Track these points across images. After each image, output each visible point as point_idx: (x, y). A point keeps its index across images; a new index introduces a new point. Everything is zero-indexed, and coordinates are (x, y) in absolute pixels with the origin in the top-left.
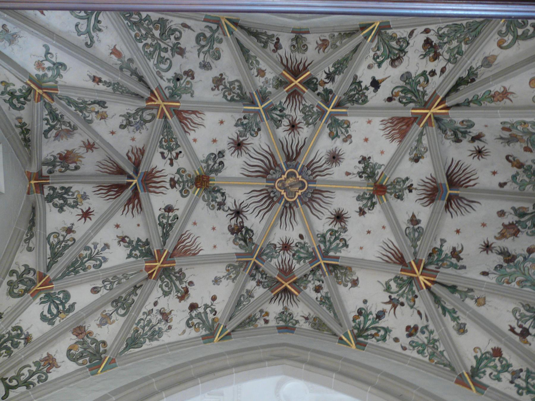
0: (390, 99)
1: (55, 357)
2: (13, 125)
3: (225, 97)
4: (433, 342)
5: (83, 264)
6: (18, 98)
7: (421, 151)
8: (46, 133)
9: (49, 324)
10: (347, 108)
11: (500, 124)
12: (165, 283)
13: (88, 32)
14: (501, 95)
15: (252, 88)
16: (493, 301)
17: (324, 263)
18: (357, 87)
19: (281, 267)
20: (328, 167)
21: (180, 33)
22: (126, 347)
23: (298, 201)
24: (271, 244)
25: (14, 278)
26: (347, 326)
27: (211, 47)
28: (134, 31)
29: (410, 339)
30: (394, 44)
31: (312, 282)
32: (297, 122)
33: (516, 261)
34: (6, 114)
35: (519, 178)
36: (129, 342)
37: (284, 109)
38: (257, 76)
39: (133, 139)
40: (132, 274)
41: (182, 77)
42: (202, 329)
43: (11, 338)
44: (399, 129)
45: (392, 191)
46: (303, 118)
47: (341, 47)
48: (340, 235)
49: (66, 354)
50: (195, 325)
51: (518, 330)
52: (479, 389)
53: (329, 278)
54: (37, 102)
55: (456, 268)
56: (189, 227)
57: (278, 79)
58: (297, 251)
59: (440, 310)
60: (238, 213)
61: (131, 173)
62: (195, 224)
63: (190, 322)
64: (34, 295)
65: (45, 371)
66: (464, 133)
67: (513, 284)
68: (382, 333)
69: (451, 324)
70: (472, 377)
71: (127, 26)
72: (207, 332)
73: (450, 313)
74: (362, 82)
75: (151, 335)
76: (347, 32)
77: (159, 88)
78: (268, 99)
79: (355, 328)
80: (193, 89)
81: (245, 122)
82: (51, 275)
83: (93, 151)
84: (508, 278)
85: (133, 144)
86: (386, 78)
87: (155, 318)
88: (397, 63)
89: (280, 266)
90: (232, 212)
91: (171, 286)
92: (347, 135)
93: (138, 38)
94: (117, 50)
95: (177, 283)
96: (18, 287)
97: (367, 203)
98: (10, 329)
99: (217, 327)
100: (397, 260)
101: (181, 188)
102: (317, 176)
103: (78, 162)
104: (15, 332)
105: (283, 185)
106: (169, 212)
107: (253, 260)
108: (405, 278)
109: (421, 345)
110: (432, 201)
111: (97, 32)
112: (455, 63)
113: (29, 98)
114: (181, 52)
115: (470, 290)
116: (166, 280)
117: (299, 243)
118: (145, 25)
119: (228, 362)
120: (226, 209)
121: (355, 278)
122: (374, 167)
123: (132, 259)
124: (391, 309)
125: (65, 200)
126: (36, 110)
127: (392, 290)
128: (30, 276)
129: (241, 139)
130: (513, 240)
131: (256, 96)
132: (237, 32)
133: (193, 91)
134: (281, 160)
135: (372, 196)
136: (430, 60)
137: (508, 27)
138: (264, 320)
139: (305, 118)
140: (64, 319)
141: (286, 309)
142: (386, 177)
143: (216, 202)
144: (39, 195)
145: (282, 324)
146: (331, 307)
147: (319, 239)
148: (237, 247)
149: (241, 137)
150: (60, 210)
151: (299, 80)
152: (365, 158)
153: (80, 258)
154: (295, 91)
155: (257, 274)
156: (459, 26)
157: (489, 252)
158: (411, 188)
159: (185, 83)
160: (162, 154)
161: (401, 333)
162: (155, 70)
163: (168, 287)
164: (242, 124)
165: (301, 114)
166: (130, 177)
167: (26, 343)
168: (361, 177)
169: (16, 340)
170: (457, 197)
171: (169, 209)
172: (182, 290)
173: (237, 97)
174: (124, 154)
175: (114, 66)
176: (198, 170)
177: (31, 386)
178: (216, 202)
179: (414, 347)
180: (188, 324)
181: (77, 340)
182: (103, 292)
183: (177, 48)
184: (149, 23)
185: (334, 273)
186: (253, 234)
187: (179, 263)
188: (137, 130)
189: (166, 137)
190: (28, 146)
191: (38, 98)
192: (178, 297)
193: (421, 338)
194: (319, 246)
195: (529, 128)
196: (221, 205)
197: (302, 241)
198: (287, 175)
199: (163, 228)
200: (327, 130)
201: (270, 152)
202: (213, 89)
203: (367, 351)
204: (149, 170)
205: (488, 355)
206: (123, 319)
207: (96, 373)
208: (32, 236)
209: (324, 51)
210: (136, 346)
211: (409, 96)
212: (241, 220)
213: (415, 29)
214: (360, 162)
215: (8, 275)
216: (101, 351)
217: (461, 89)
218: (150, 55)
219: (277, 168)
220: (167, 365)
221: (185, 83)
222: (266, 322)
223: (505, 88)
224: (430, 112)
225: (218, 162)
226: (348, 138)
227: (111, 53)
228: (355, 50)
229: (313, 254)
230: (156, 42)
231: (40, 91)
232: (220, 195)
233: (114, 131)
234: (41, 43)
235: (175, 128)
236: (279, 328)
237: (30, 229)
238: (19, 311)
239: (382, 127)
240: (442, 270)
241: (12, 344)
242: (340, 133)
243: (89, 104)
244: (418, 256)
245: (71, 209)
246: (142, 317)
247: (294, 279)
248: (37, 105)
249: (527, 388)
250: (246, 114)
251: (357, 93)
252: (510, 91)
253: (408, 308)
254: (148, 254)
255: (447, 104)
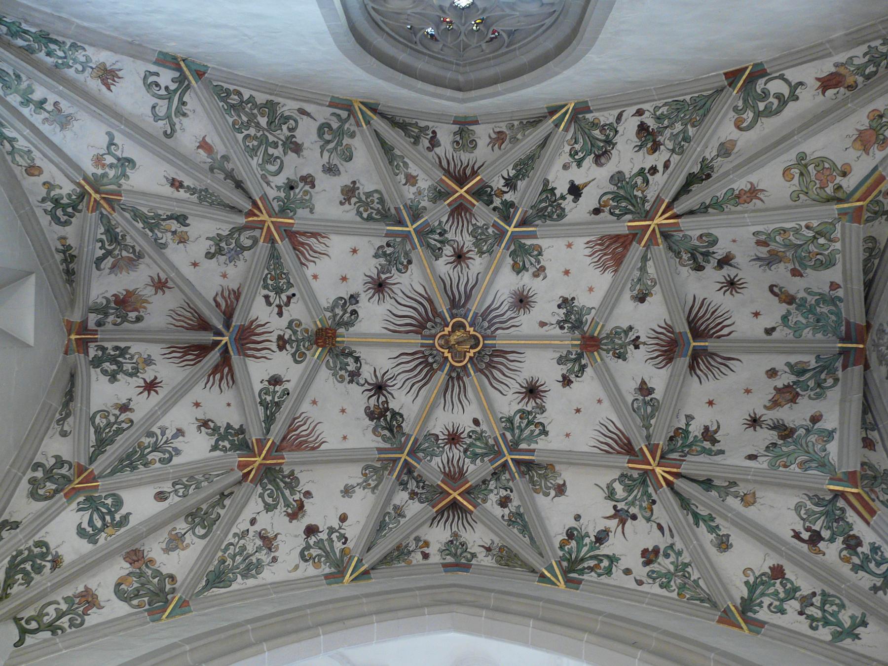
0: (597, 211)
1: (96, 593)
2: (53, 249)
3: (359, 214)
4: (682, 569)
5: (143, 456)
6: (64, 208)
7: (645, 284)
8: (99, 261)
9: (89, 542)
10: (537, 226)
11: (752, 236)
12: (269, 491)
13: (168, 117)
14: (748, 195)
15: (398, 201)
16: (766, 496)
17: (512, 459)
18: (549, 196)
19: (447, 469)
20: (513, 315)
21: (296, 121)
22: (207, 585)
23: (469, 366)
24: (430, 434)
25: (39, 474)
26: (550, 554)
27: (340, 143)
28: (232, 116)
29: (648, 568)
30: (597, 133)
31: (495, 492)
32: (465, 250)
33: (795, 436)
34: (45, 231)
35: (792, 319)
36: (212, 577)
37: (445, 231)
38: (405, 184)
39: (224, 276)
40: (218, 475)
41: (298, 184)
42: (325, 565)
43: (31, 557)
44: (613, 253)
45: (610, 347)
46: (474, 244)
47: (522, 140)
48: (535, 417)
49: (113, 590)
50: (314, 559)
51: (806, 535)
52: (752, 627)
53: (520, 482)
54: (92, 212)
55: (710, 455)
56: (305, 407)
57: (435, 189)
58: (470, 445)
59: (690, 518)
60: (379, 388)
61: (220, 327)
62: (314, 402)
63: (306, 553)
64: (71, 495)
65: (81, 612)
66: (707, 255)
67: (792, 467)
68: (605, 563)
69: (707, 537)
70: (743, 613)
71: (222, 109)
72: (333, 570)
73: (704, 521)
74: (556, 188)
75: (244, 570)
76: (532, 120)
77: (265, 197)
78: (423, 217)
79: (563, 558)
80: (313, 201)
81: (389, 250)
82: (96, 467)
83: (164, 293)
84: (785, 459)
85: (225, 283)
86: (590, 182)
87: (253, 544)
88: (603, 160)
89: (444, 468)
90: (370, 387)
91: (278, 496)
92: (538, 267)
93: (237, 127)
94: (207, 143)
95: (287, 492)
96: (45, 486)
97: (573, 367)
98: (31, 543)
99: (348, 562)
100: (622, 448)
101: (294, 350)
102: (497, 329)
103: (141, 310)
104: (38, 549)
105: (447, 342)
106: (275, 385)
107: (404, 456)
108: (635, 475)
109: (665, 575)
110: (670, 360)
111: (181, 118)
112: (681, 153)
113: (80, 207)
114: (297, 149)
115: (733, 484)
116: (270, 486)
117: (473, 432)
118: (247, 109)
119: (365, 609)
120: (362, 381)
121: (561, 482)
122: (580, 313)
123: (218, 453)
124: (618, 526)
125: (120, 365)
126: (88, 225)
127: (617, 497)
128: (64, 471)
129: (383, 276)
130: (791, 408)
131: (404, 212)
132: (378, 123)
133: (313, 205)
134: (443, 306)
135: (580, 356)
136: (648, 154)
137: (745, 101)
138: (422, 552)
139: (476, 245)
140: (113, 536)
141: (455, 535)
142: (598, 323)
143: (347, 371)
144: (82, 355)
145: (450, 559)
146: (525, 529)
147: (504, 424)
148: (380, 439)
149: (383, 273)
150: (112, 379)
151: (465, 188)
152: (567, 299)
153: (139, 447)
154: (461, 204)
155: (410, 482)
156: (681, 103)
157: (758, 428)
158: (637, 343)
159: (301, 194)
160: (267, 297)
161: (633, 560)
162: (259, 172)
163: (272, 497)
164: (385, 255)
165: (471, 238)
166: (219, 333)
167: (53, 568)
168: (562, 328)
169: (39, 562)
170: (704, 350)
171: (275, 380)
172: (294, 503)
173: (376, 215)
174: (210, 297)
175: (202, 165)
176: (320, 320)
177: (59, 632)
178: (347, 371)
179: (654, 579)
180: (302, 556)
181: (131, 570)
182: (173, 499)
183: (291, 142)
184: (253, 108)
185: (527, 476)
186: (403, 419)
187: (289, 460)
188: (230, 262)
189: (273, 273)
190: (70, 282)
191: (93, 207)
192: (288, 515)
193: (665, 564)
194: (504, 434)
195: (791, 238)
196: (354, 376)
197: (478, 429)
198: (452, 327)
199: (266, 408)
200: (509, 261)
201: (426, 296)
202: (341, 203)
203: (582, 590)
204: (247, 324)
205: (764, 578)
206: (204, 542)
207: (160, 619)
208: (68, 415)
209: (500, 148)
210: (221, 585)
211: (624, 204)
212: (384, 399)
213: (624, 111)
214: (559, 306)
215: (30, 469)
216: (167, 590)
217: (693, 189)
218: (253, 151)
219: (438, 320)
220: (269, 609)
221: (301, 194)
222: (426, 556)
223: (751, 183)
224: (653, 224)
225: (349, 310)
226: (540, 271)
227: (198, 147)
228: (544, 144)
229: (496, 448)
230: (261, 133)
231: (97, 197)
232: (352, 360)
233: (197, 262)
234: (105, 128)
235: (287, 256)
236: (445, 566)
237: (66, 405)
238: (44, 519)
239: (588, 251)
240: (689, 458)
241: (32, 566)
242: (529, 263)
243: (164, 220)
244: (653, 439)
245: (129, 379)
246: (232, 541)
247: (467, 486)
248: (91, 217)
249: (824, 618)
250: (390, 239)
251: (550, 205)
252: (759, 188)
253: (644, 521)
254: (244, 446)
255: (676, 210)
